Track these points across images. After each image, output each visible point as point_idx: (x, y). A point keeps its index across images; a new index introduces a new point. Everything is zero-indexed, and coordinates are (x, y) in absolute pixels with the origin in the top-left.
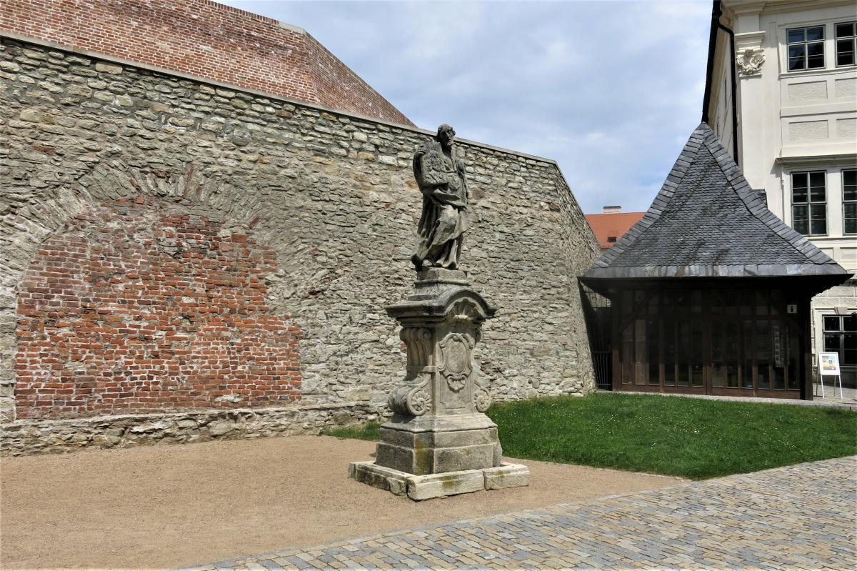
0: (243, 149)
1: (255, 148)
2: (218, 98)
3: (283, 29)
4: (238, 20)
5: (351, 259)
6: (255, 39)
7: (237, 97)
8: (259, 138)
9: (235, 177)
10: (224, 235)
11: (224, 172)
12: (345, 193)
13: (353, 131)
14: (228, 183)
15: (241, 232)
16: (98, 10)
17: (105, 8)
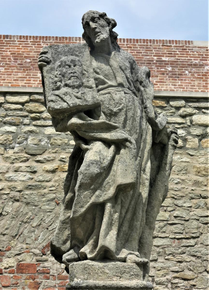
0: (39, 158)
1: (54, 155)
2: (8, 106)
3: (198, 47)
4: (148, 49)
5: (192, 282)
6: (166, 63)
7: (31, 101)
8: (59, 142)
9: (27, 192)
10: (6, 266)
11: (12, 189)
12: (181, 194)
13: (191, 115)
14: (18, 201)
15: (29, 259)
16: (8, 72)
17: (15, 68)
